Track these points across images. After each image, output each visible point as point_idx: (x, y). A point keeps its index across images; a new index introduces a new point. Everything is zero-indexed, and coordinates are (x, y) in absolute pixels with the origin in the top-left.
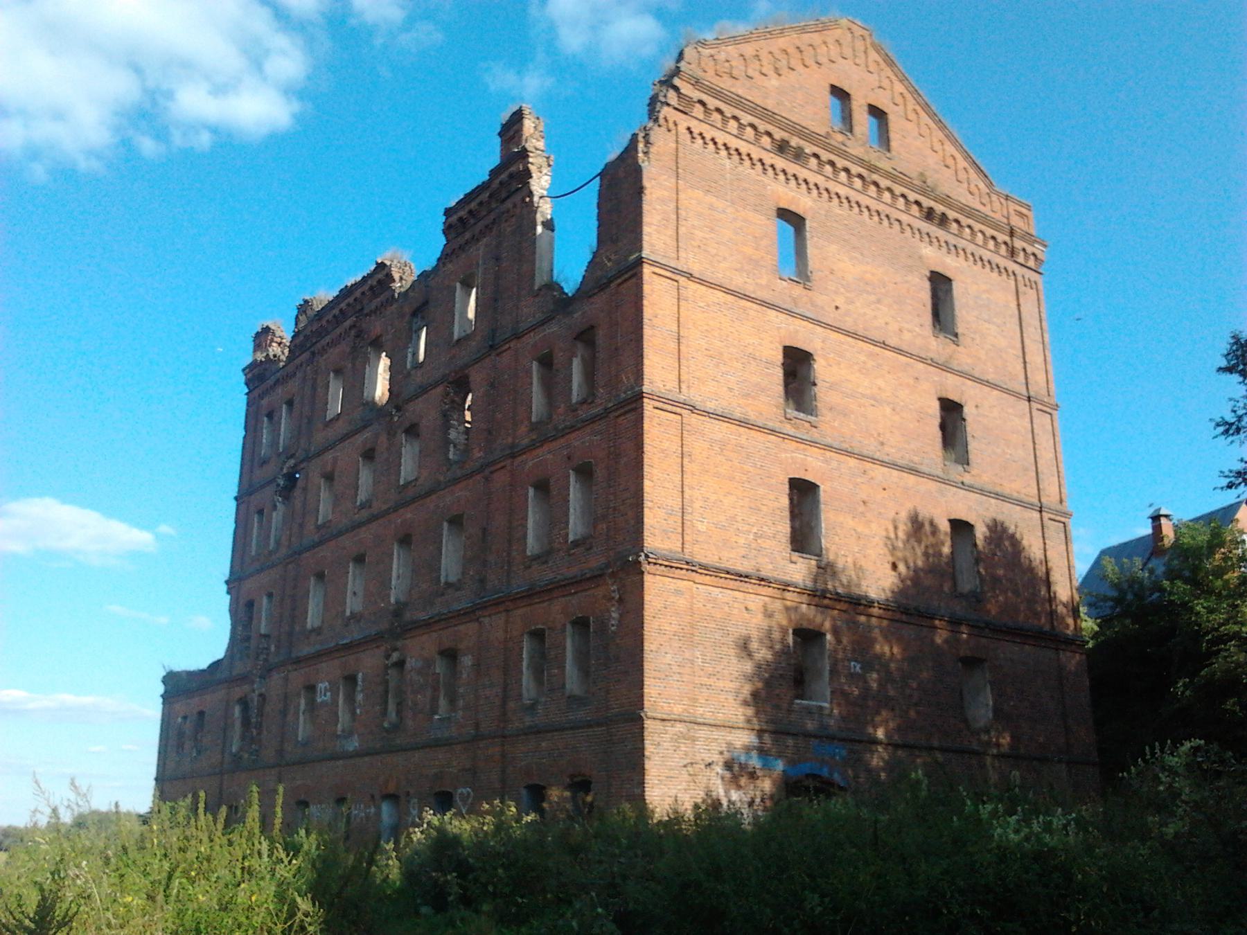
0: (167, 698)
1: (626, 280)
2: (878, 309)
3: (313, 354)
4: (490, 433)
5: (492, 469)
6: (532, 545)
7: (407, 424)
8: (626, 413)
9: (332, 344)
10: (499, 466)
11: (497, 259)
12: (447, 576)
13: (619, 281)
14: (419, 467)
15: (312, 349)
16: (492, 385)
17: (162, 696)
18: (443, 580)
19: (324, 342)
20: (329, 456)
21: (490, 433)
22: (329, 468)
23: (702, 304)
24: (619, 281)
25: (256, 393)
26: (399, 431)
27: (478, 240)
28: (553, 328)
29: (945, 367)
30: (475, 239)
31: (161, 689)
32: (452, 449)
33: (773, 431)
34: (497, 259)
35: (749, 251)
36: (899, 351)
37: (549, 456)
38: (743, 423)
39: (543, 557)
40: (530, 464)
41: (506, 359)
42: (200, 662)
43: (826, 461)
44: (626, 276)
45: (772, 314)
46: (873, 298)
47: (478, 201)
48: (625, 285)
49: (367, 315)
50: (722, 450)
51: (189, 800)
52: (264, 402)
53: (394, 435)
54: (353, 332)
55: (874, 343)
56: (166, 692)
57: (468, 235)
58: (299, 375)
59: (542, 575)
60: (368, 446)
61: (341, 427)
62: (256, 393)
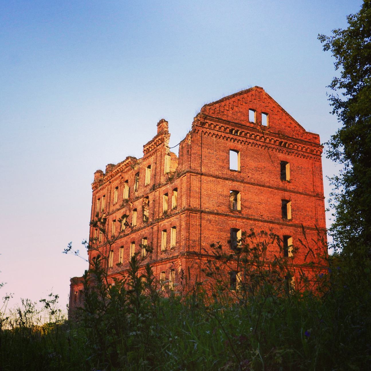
0: (72, 286)
1: (184, 176)
2: (263, 175)
3: (110, 182)
4: (153, 214)
5: (153, 225)
6: (163, 248)
7: (134, 208)
8: (183, 214)
9: (116, 180)
10: (155, 224)
11: (156, 163)
12: (143, 254)
13: (183, 176)
14: (137, 222)
15: (110, 181)
16: (154, 200)
17: (70, 285)
18: (142, 256)
19: (113, 179)
20: (114, 215)
21: (153, 214)
22: (114, 219)
23: (205, 182)
24: (183, 176)
25: (95, 192)
26: (132, 210)
27: (151, 156)
28: (168, 186)
29: (285, 190)
30: (151, 156)
31: (70, 283)
32: (144, 217)
33: (226, 215)
34: (156, 163)
35: (221, 164)
36: (269, 187)
37: (166, 223)
38: (217, 214)
39: (165, 251)
40: (162, 225)
41: (157, 193)
42: (80, 274)
43: (243, 222)
44: (184, 175)
45: (227, 182)
46: (261, 172)
47: (151, 144)
48: (184, 178)
49: (124, 173)
50: (210, 222)
51: (267, 242)
52: (97, 195)
53: (131, 211)
54: (121, 177)
55: (260, 186)
56: (71, 284)
57: (149, 154)
58: (107, 188)
59: (164, 256)
60: (124, 214)
61: (118, 206)
62: (95, 192)
